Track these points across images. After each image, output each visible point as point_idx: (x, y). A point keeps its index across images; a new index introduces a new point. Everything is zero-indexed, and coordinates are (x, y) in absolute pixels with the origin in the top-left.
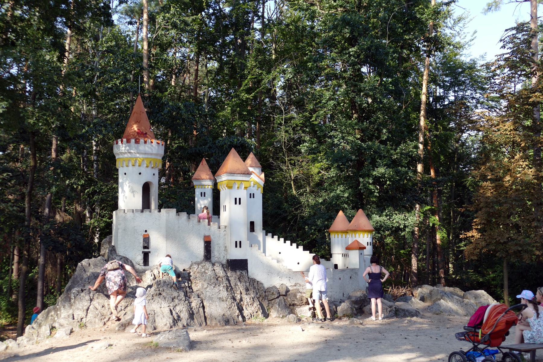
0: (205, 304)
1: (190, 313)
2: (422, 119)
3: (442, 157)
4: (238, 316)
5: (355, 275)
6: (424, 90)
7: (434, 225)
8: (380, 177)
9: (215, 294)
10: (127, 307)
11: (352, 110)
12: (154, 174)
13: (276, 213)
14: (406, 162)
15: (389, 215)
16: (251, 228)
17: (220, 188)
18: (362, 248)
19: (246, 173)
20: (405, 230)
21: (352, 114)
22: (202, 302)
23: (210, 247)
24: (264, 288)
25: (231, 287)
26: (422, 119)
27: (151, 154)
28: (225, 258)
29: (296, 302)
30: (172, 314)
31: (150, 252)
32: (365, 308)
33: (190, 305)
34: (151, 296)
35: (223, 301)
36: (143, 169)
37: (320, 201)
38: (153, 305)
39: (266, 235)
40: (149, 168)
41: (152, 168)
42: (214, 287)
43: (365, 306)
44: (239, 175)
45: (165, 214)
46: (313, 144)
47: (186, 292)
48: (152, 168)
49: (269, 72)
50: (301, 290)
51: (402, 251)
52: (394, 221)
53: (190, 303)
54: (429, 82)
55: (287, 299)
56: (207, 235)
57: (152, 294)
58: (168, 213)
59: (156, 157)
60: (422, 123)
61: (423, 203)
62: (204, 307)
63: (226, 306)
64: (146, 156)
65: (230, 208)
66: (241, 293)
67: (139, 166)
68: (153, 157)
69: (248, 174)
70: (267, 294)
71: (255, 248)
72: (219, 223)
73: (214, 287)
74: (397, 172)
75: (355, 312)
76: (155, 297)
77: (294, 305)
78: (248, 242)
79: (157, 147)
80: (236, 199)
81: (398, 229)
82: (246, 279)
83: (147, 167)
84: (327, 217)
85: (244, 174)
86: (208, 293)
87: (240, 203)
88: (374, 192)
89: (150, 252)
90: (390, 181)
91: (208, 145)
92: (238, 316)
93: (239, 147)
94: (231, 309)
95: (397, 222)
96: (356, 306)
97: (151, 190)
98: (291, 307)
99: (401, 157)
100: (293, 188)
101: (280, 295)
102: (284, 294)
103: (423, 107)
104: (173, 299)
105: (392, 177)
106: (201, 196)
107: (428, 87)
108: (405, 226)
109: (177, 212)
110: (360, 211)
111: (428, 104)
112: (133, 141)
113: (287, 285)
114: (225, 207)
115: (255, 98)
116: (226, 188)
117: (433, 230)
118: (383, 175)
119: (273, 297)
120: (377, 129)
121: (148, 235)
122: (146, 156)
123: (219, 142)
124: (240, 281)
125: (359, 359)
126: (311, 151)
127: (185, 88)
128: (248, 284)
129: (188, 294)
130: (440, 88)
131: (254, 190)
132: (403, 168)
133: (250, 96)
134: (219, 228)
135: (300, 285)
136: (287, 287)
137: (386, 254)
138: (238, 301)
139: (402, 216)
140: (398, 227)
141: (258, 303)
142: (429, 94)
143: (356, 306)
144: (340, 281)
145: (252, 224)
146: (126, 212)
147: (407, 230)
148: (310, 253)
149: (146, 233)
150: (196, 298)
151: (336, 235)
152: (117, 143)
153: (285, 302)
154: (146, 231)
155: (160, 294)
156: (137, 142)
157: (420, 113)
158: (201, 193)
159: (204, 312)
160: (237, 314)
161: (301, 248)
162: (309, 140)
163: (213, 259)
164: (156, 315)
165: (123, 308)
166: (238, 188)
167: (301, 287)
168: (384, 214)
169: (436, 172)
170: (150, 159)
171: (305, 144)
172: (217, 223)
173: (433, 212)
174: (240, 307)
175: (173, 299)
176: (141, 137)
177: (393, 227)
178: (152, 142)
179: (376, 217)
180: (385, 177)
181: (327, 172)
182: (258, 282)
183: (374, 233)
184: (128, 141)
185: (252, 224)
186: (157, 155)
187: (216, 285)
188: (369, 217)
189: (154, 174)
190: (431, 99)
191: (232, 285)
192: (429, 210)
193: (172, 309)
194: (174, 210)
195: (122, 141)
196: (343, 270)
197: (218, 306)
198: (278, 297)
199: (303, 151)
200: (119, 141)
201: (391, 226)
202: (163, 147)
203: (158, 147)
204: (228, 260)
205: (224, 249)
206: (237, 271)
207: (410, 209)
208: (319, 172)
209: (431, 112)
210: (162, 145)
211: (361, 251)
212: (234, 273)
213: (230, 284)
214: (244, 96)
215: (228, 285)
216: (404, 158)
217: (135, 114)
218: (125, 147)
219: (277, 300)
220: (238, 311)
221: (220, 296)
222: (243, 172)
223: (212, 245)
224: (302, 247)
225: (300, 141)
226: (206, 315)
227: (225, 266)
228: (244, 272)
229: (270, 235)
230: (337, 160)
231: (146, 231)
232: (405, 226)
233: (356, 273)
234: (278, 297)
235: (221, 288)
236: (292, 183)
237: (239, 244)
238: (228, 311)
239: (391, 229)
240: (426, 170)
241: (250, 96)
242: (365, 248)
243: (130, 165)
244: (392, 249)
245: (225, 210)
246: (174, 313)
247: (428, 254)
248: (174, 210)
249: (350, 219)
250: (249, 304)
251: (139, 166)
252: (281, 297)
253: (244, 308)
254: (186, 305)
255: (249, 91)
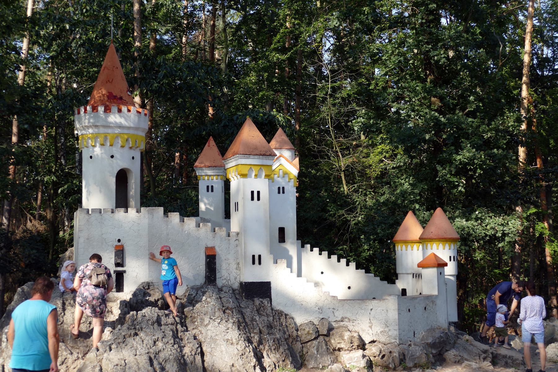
0: (204, 349)
1: (180, 363)
2: (524, 87)
3: (552, 141)
4: (255, 367)
5: (431, 305)
6: (527, 47)
7: (541, 234)
8: (467, 164)
9: (221, 334)
10: (87, 353)
11: (426, 69)
12: (133, 158)
14: (505, 142)
15: (481, 218)
16: (280, 238)
17: (230, 177)
18: (442, 265)
20: (503, 240)
21: (426, 75)
22: (200, 346)
23: (215, 264)
24: (295, 324)
25: (246, 323)
26: (524, 87)
27: (129, 128)
28: (238, 280)
29: (342, 346)
30: (152, 364)
31: (125, 272)
32: (446, 353)
33: (181, 351)
34: (121, 337)
35: (232, 344)
36: (116, 151)
38: (124, 351)
39: (303, 246)
40: (126, 149)
41: (131, 148)
42: (219, 323)
43: (447, 351)
44: (256, 157)
46: (370, 119)
47: (177, 330)
48: (131, 148)
49: (309, 24)
50: (351, 328)
51: (497, 271)
52: (488, 227)
53: (181, 348)
54: (532, 38)
55: (329, 341)
56: (210, 246)
57: (123, 334)
60: (524, 93)
61: (526, 204)
62: (202, 354)
63: (236, 352)
65: (244, 205)
66: (261, 332)
67: (111, 145)
68: (132, 132)
70: (299, 333)
71: (283, 264)
72: (229, 229)
73: (219, 323)
74: (492, 157)
75: (433, 361)
76: (128, 339)
77: (339, 350)
78: (272, 256)
79: (137, 118)
81: (494, 239)
82: (269, 311)
83: (122, 147)
85: (264, 155)
86: (209, 333)
88: (458, 186)
89: (125, 272)
90: (481, 169)
91: (223, 123)
92: (255, 367)
94: (244, 357)
95: (492, 228)
96: (434, 352)
97: (129, 181)
98: (337, 352)
99: (497, 135)
100: (344, 182)
101: (319, 336)
102: (325, 333)
103: (525, 71)
104: (155, 342)
105: (484, 162)
107: (532, 45)
108: (504, 235)
110: (439, 210)
111: (532, 68)
112: (101, 109)
113: (330, 320)
116: (239, 176)
117: (540, 241)
118: (471, 160)
119: (309, 338)
120: (462, 96)
121: (122, 246)
123: (237, 118)
124: (259, 314)
125: (437, 334)
126: (367, 129)
127: (197, 48)
128: (271, 318)
129: (179, 335)
130: (548, 47)
132: (500, 151)
133: (284, 57)
134: (229, 236)
135: (349, 320)
136: (329, 323)
137: (475, 274)
138: (255, 344)
139: (500, 220)
140: (494, 235)
141: (286, 347)
142: (533, 54)
143: (434, 352)
144: (409, 314)
145: (282, 231)
146: (90, 212)
147: (507, 239)
148: (366, 272)
149: (120, 244)
150: (192, 340)
151: (404, 247)
152: (79, 113)
153: (326, 345)
154: (119, 241)
155: (136, 334)
156: (107, 110)
157: (521, 79)
158: (208, 187)
159: (203, 361)
160: (253, 364)
161: (353, 265)
162: (365, 114)
163: (220, 282)
164: (127, 366)
165: (80, 356)
167: (351, 324)
168: (474, 216)
169: (545, 162)
171: (359, 120)
172: (224, 229)
173: (540, 217)
174: (259, 354)
175: (155, 342)
177: (486, 235)
178: (129, 111)
179: (461, 222)
180: (474, 163)
182: (286, 315)
183: (459, 244)
185: (282, 231)
186: (136, 129)
187: (222, 320)
188: (452, 219)
189: (133, 158)
190: (535, 61)
191: (247, 320)
192: (534, 214)
193: (152, 356)
194: (161, 209)
195: (86, 110)
196: (413, 298)
197: (224, 352)
198: (316, 338)
199: (356, 129)
200: (82, 109)
201: (483, 235)
203: (139, 118)
204: (241, 284)
205: (235, 266)
206: (256, 299)
207: (509, 211)
209: (534, 81)
210: (146, 115)
211: (440, 269)
212: (250, 302)
213: (244, 319)
214: (276, 57)
215: (241, 320)
216: (501, 136)
219: (315, 342)
220: (255, 360)
221: (229, 336)
222: (262, 153)
223: (217, 261)
224: (327, 252)
225: (352, 114)
226: (206, 365)
227: (237, 292)
228: (265, 302)
229: (308, 246)
230: (404, 139)
231: (119, 241)
232: (504, 235)
233: (433, 302)
234: (316, 338)
235: (230, 325)
236: (342, 175)
237: (257, 260)
238: (240, 360)
239: (483, 238)
240: (530, 159)
241: (284, 57)
242: (446, 265)
244: (484, 268)
245: (237, 209)
246: (155, 363)
247: (531, 274)
249: (424, 223)
250: (272, 349)
251: (111, 145)
252: (321, 338)
253: (265, 354)
254: (174, 351)
255: (283, 50)
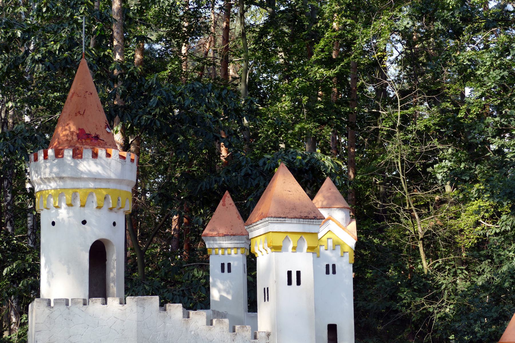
12: (114, 224)
13: (388, 308)
19: (312, 216)
27: (108, 180)
36: (89, 214)
37: (480, 284)
40: (105, 210)
41: (111, 209)
44: (295, 221)
45: (135, 309)
46: (460, 162)
48: (111, 209)
49: (367, 24)
58: (142, 306)
59: (118, 187)
64: (98, 185)
67: (83, 206)
68: (112, 186)
69: (315, 218)
72: (255, 327)
79: (119, 166)
80: (299, 283)
83: (99, 207)
84: (495, 315)
85: (306, 218)
87: (289, 273)
93: (307, 171)
106: (223, 271)
109: (162, 305)
112: (68, 153)
114: (266, 291)
115: (341, 77)
116: (269, 250)
122: (98, 185)
123: (265, 164)
131: (332, 257)
133: (331, 73)
134: (255, 338)
146: (52, 304)
152: (36, 159)
156: (77, 155)
158: (223, 265)
166: (294, 248)
170: (104, 193)
171: (443, 164)
172: (248, 327)
176: (87, 144)
178: (108, 155)
181: (494, 223)
184: (58, 153)
185: (332, 329)
186: (119, 181)
189: (114, 224)
194: (156, 300)
202: (135, 165)
203: (123, 165)
208: (478, 224)
210: (132, 160)
217: (75, 98)
218: (51, 167)
236: (420, 245)
241: (331, 73)
243: (64, 205)
245: (266, 297)
248: (156, 300)
251: (83, 206)
255: (329, 63)
